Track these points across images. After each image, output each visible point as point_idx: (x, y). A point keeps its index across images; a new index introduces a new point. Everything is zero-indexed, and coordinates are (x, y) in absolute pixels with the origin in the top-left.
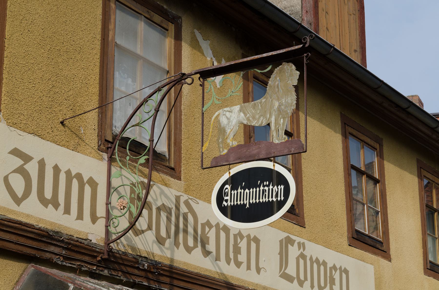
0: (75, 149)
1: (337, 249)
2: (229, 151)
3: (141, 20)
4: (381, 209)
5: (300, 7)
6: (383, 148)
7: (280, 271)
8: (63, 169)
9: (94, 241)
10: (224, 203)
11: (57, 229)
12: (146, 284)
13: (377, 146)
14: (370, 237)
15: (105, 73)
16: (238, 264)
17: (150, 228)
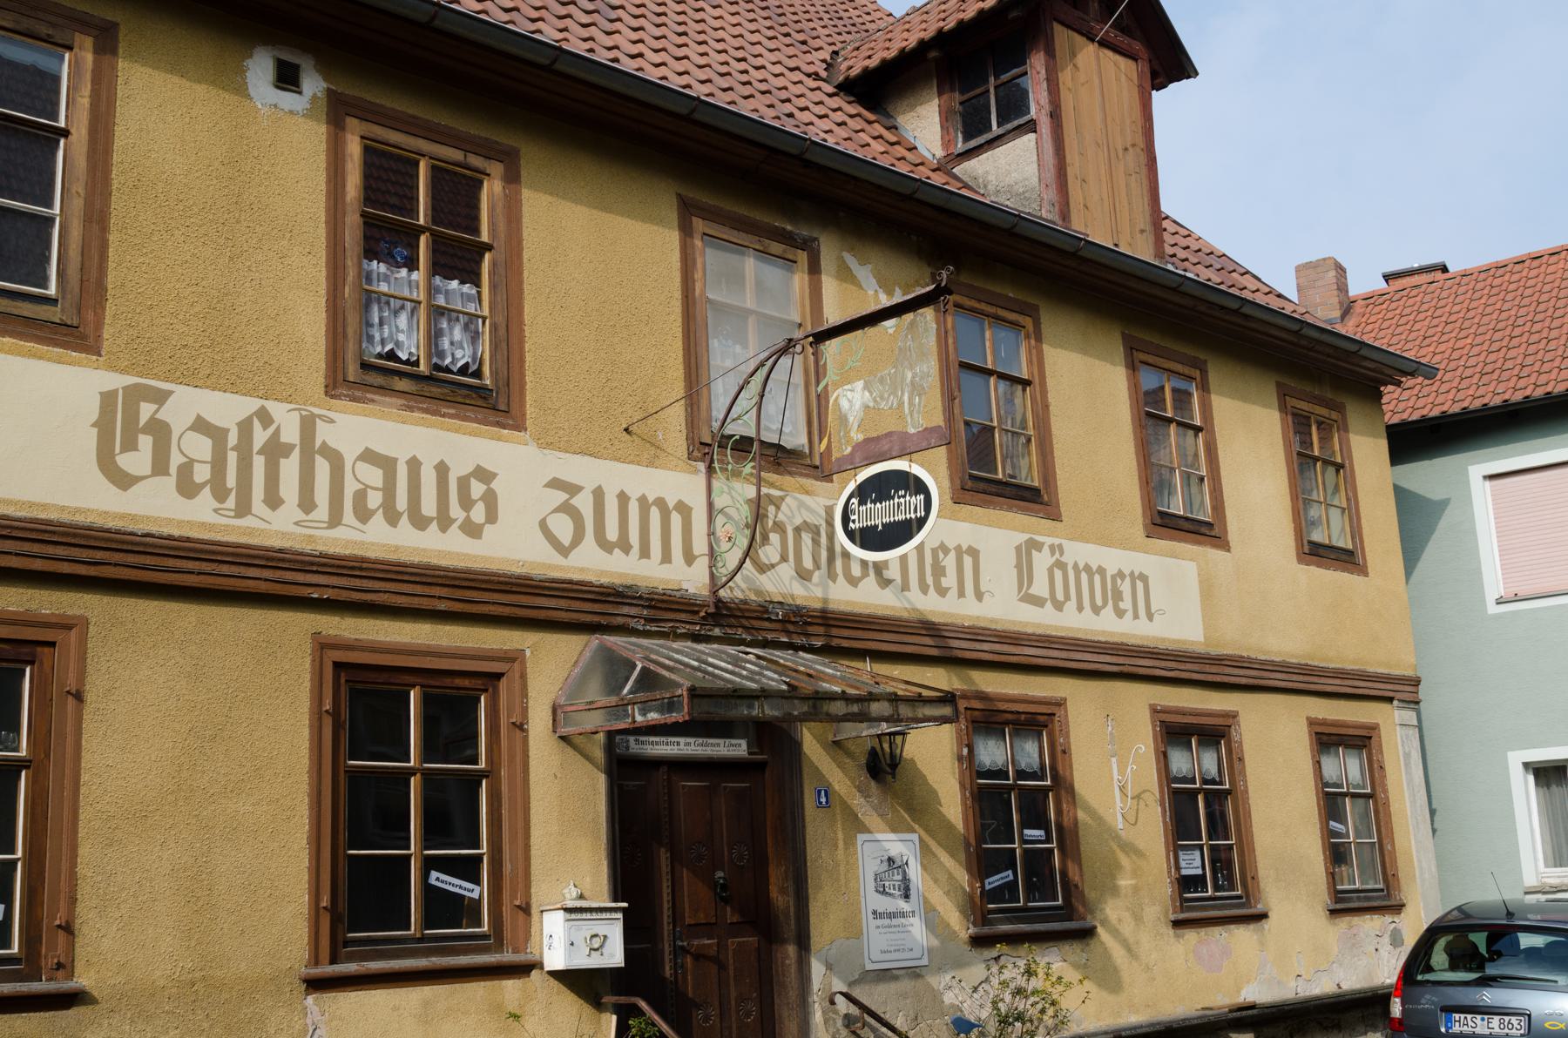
0: (650, 464)
1: (1125, 544)
2: (854, 448)
3: (749, 256)
4: (1207, 472)
5: (1037, 180)
6: (1207, 376)
7: (1020, 592)
8: (634, 495)
9: (692, 591)
10: (851, 524)
11: (630, 582)
12: (785, 640)
13: (1197, 374)
14: (1187, 519)
15: (692, 344)
16: (942, 592)
17: (784, 559)
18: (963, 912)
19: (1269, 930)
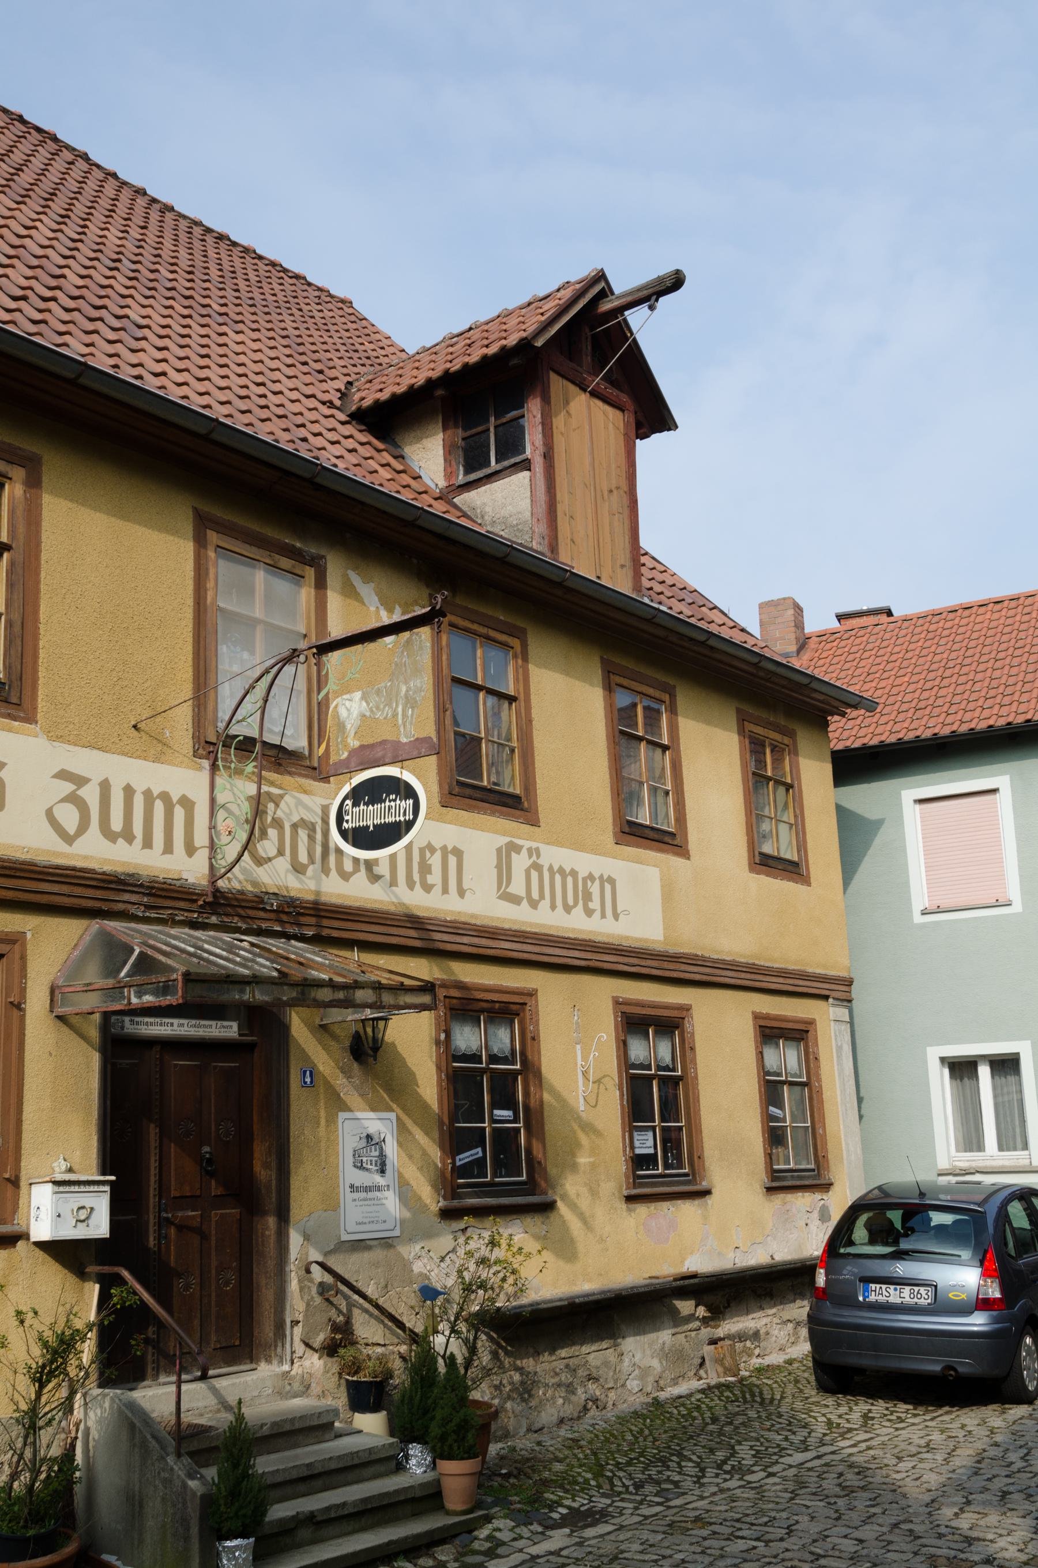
18: (434, 1186)
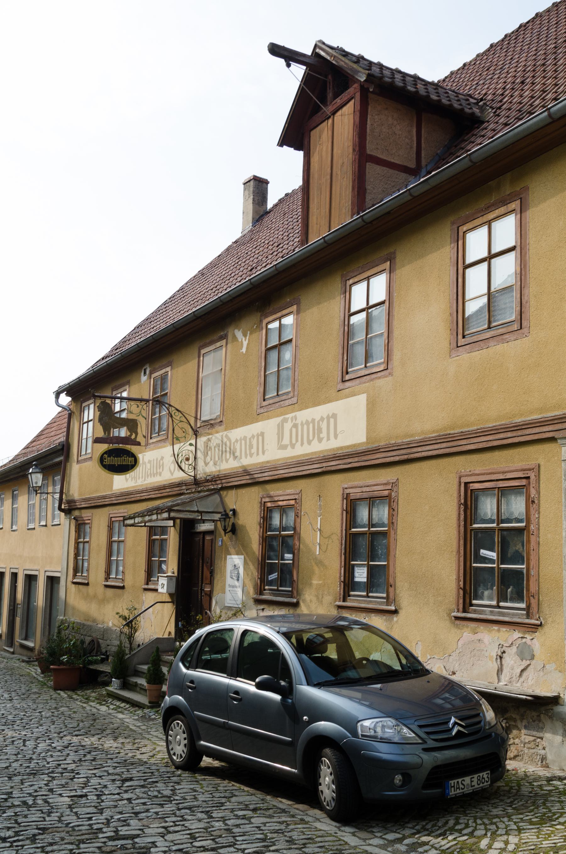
18: (254, 588)
19: (397, 621)
